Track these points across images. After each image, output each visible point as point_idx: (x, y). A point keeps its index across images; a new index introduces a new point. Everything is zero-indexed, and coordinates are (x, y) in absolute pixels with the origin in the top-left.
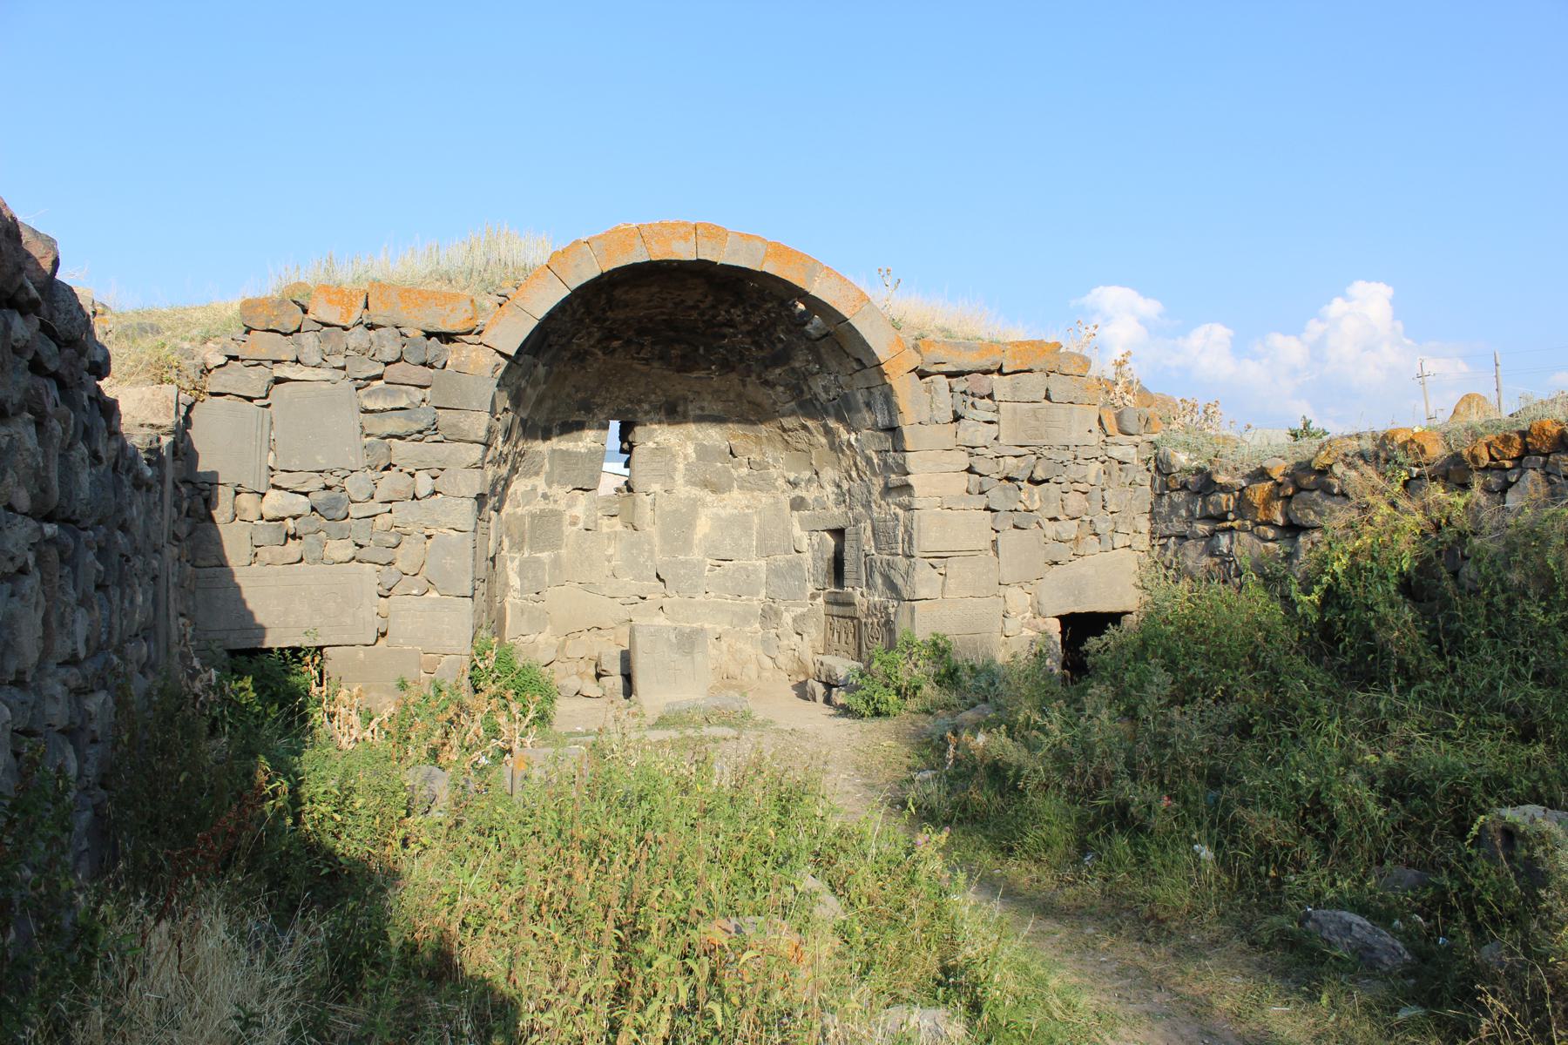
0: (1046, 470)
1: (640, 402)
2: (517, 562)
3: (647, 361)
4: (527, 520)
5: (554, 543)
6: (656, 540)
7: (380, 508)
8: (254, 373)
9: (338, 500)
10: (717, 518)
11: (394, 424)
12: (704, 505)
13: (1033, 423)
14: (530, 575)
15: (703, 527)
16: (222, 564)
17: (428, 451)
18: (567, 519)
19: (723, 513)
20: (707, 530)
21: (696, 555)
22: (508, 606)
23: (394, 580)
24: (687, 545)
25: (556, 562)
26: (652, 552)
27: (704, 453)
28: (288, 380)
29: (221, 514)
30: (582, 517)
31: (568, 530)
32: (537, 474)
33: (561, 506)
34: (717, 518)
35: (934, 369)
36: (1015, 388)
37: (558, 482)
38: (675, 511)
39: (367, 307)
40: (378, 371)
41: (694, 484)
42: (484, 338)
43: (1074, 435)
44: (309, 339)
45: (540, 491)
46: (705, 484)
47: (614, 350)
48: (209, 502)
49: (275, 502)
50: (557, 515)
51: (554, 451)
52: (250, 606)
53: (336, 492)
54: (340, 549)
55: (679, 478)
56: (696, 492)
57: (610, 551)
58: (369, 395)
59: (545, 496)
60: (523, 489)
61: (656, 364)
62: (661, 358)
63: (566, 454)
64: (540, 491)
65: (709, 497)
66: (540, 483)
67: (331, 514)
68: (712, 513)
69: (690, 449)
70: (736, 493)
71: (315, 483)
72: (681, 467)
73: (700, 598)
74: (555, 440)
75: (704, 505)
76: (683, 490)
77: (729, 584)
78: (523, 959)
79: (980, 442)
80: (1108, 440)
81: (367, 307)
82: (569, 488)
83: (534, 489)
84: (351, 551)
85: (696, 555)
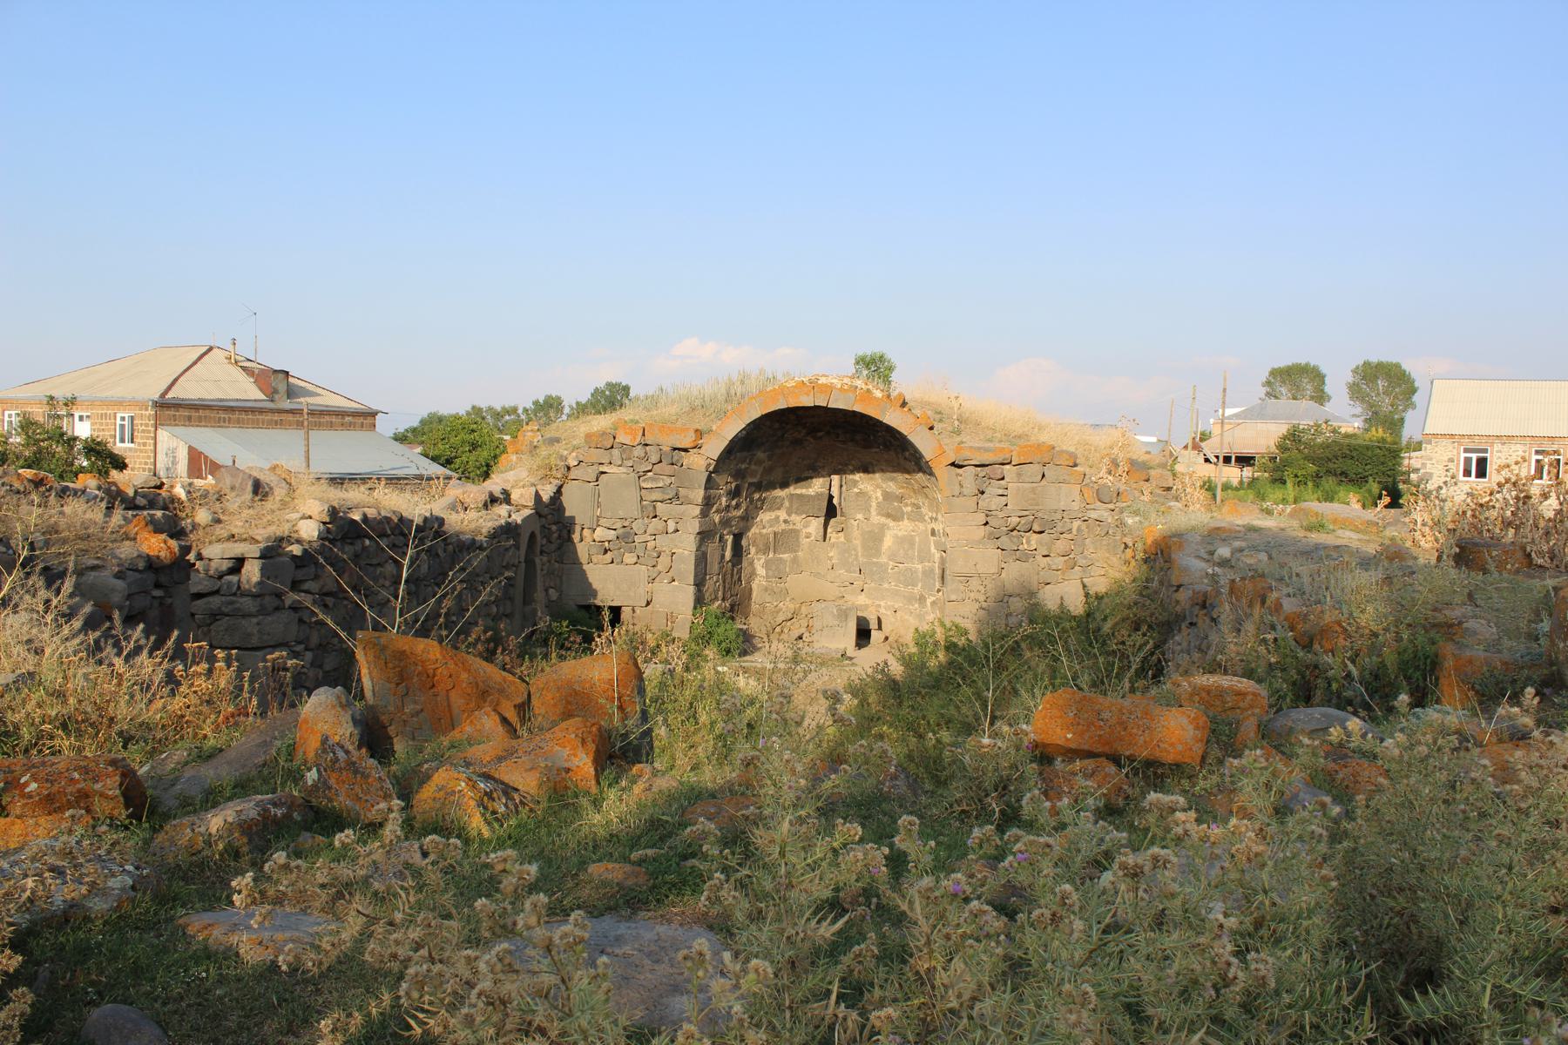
0: (1040, 526)
1: (846, 465)
2: (762, 561)
3: (844, 442)
4: (772, 536)
5: (793, 549)
6: (859, 549)
7: (649, 538)
8: (590, 469)
9: (629, 533)
10: (896, 536)
11: (656, 496)
12: (888, 528)
13: (1033, 496)
14: (774, 568)
15: (888, 542)
16: (576, 562)
17: (675, 509)
18: (803, 534)
19: (900, 534)
20: (890, 544)
21: (883, 559)
22: (754, 586)
23: (655, 575)
24: (878, 553)
25: (795, 560)
26: (857, 555)
27: (887, 496)
28: (605, 473)
29: (576, 537)
30: (814, 533)
31: (804, 541)
32: (779, 509)
33: (798, 526)
34: (896, 536)
35: (965, 463)
36: (1019, 475)
37: (796, 513)
38: (870, 532)
39: (644, 435)
40: (650, 468)
41: (883, 515)
42: (701, 451)
43: (1062, 503)
44: (615, 452)
45: (782, 519)
46: (888, 516)
47: (821, 438)
48: (570, 532)
49: (600, 533)
50: (796, 532)
51: (792, 495)
52: (590, 580)
53: (628, 529)
54: (630, 558)
55: (873, 512)
56: (883, 520)
57: (831, 554)
58: (644, 481)
59: (785, 521)
60: (768, 518)
61: (850, 444)
62: (852, 440)
63: (800, 496)
64: (782, 519)
65: (892, 524)
66: (782, 515)
67: (626, 540)
68: (896, 531)
69: (879, 494)
70: (906, 521)
71: (618, 525)
72: (874, 504)
73: (886, 585)
74: (792, 488)
75: (888, 528)
76: (876, 519)
77: (902, 578)
78: (1247, 877)
79: (993, 508)
80: (1088, 506)
81: (644, 435)
82: (804, 516)
83: (778, 517)
84: (635, 559)
85: (883, 559)
